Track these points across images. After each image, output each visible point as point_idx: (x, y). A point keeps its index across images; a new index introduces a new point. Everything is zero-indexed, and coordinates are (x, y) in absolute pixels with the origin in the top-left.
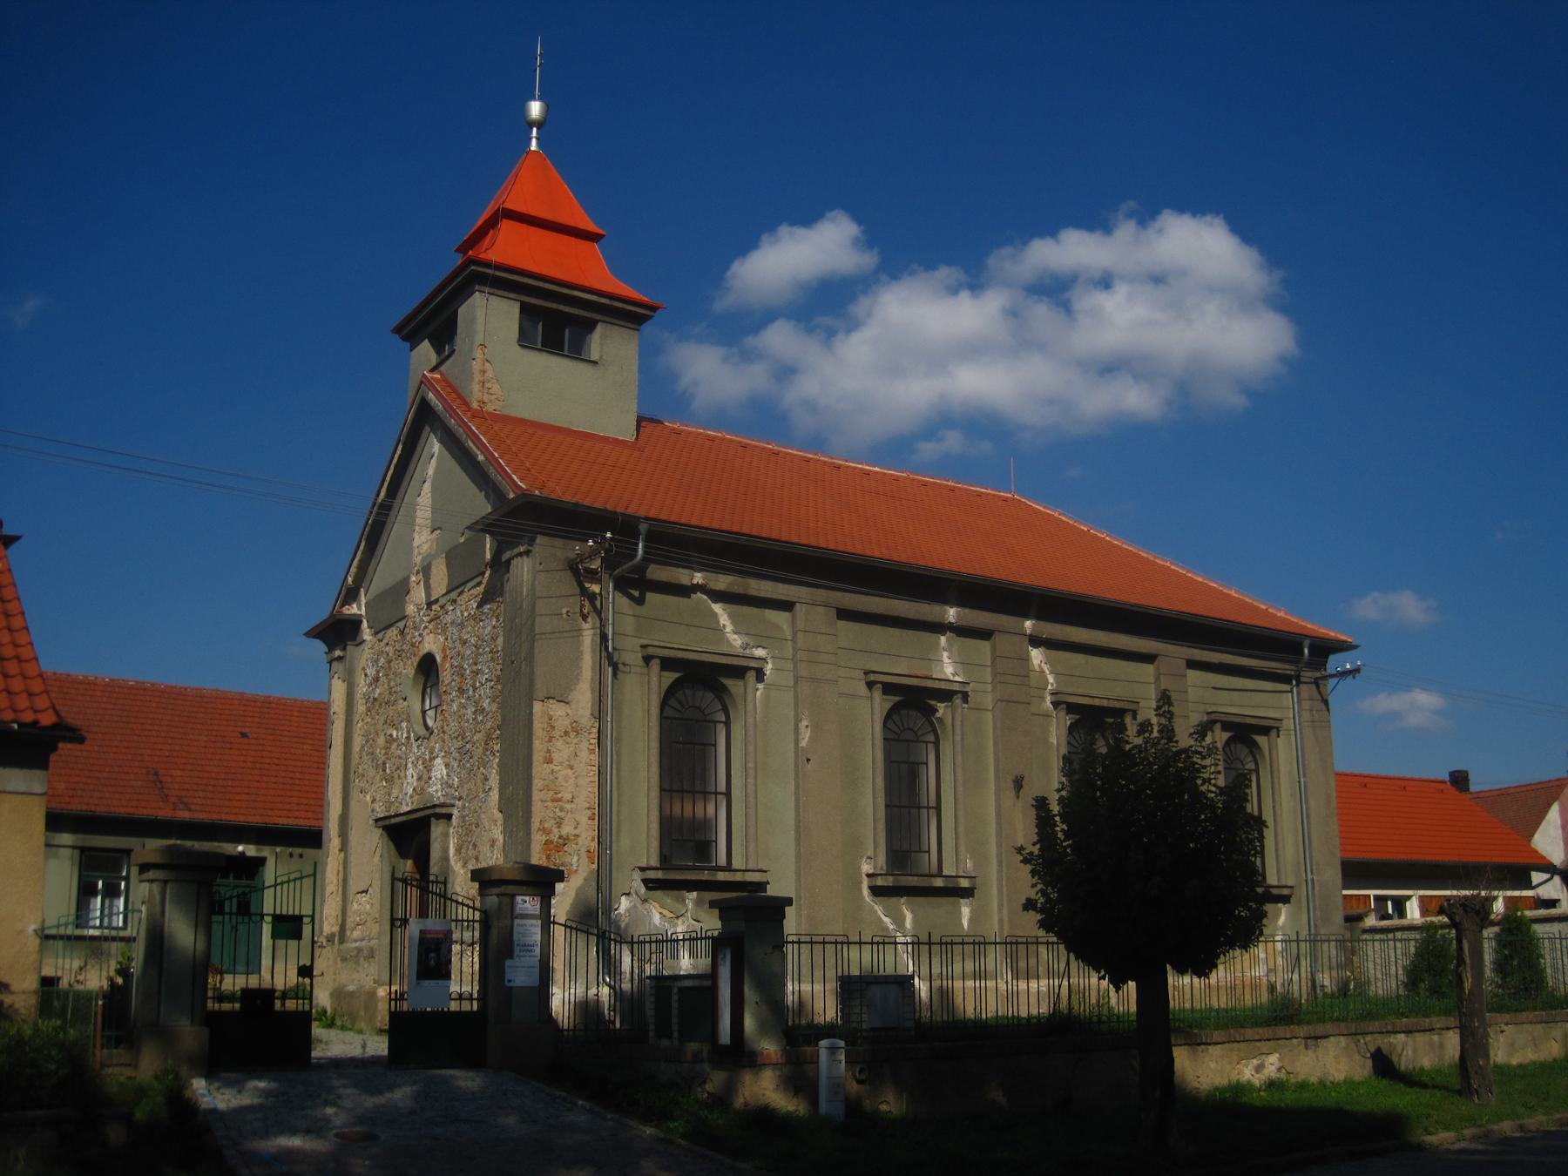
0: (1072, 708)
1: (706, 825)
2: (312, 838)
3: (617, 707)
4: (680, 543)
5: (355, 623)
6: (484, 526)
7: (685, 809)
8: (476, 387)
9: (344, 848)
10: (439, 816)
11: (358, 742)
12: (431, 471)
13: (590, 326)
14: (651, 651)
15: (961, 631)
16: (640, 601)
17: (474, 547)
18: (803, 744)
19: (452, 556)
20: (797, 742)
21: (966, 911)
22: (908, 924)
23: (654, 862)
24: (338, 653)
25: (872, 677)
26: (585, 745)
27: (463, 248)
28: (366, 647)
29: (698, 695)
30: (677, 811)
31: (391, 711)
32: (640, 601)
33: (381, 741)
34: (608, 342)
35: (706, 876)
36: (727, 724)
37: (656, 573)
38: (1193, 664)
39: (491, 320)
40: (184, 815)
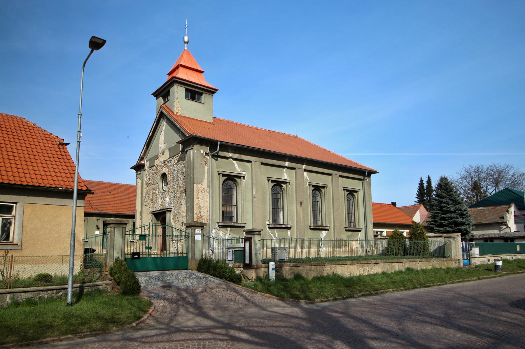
0: (313, 186)
1: (231, 213)
2: (133, 217)
3: (212, 185)
4: (226, 147)
5: (143, 166)
6: (181, 142)
7: (227, 209)
8: (175, 109)
9: (141, 219)
10: (168, 211)
11: (144, 194)
12: (164, 129)
13: (201, 94)
14: (220, 172)
15: (289, 168)
16: (217, 160)
17: (176, 147)
19: (170, 150)
20: (252, 194)
22: (277, 236)
23: (221, 221)
24: (139, 173)
26: (206, 194)
27: (169, 74)
28: (146, 171)
29: (230, 180)
30: (225, 210)
31: (154, 186)
32: (217, 160)
33: (151, 193)
34: (205, 98)
35: (232, 224)
36: (236, 189)
37: (221, 154)
38: (340, 176)
39: (178, 92)
40: (97, 211)
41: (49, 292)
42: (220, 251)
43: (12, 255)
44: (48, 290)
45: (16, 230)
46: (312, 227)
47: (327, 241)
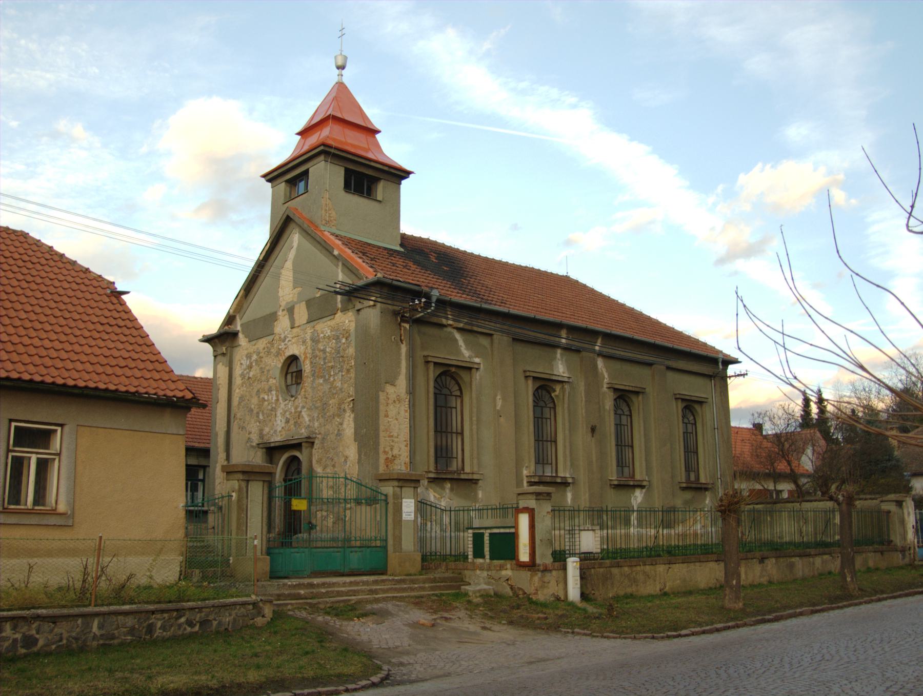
0: (615, 390)
13: (377, 180)
14: (430, 359)
18: (498, 408)
19: (309, 303)
20: (495, 406)
21: (569, 496)
25: (528, 374)
26: (403, 408)
29: (449, 380)
38: (669, 368)
41: (166, 615)
42: (448, 534)
43: (101, 537)
44: (163, 611)
45: (62, 482)
46: (684, 485)
47: (645, 513)
